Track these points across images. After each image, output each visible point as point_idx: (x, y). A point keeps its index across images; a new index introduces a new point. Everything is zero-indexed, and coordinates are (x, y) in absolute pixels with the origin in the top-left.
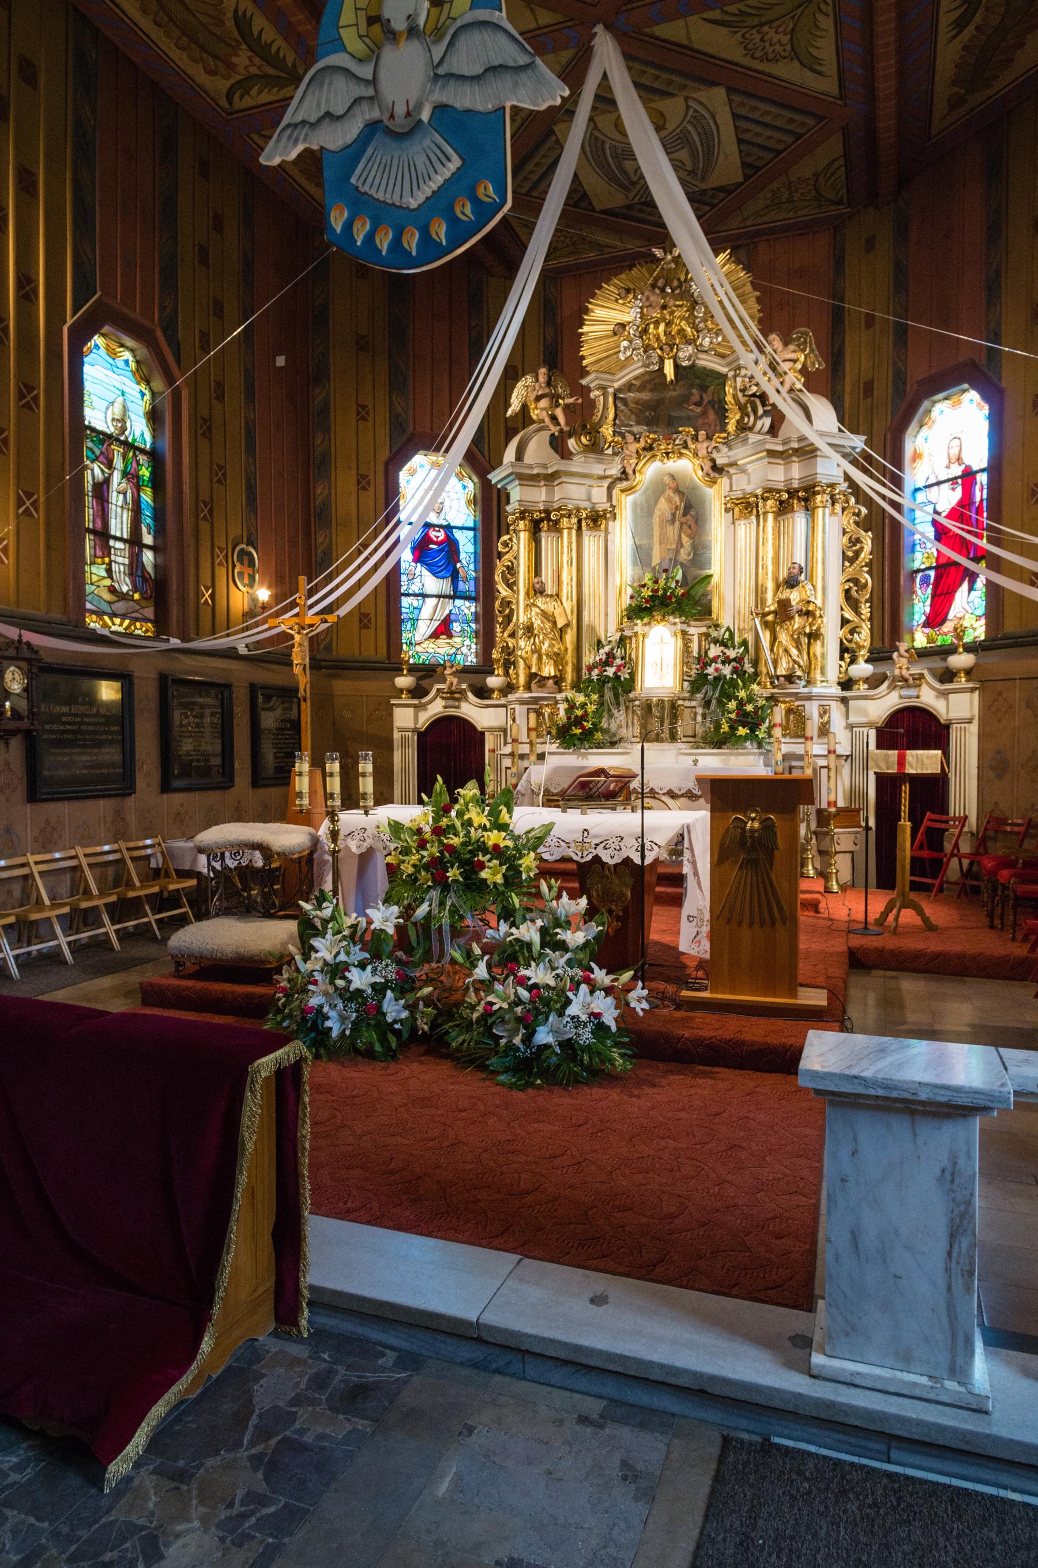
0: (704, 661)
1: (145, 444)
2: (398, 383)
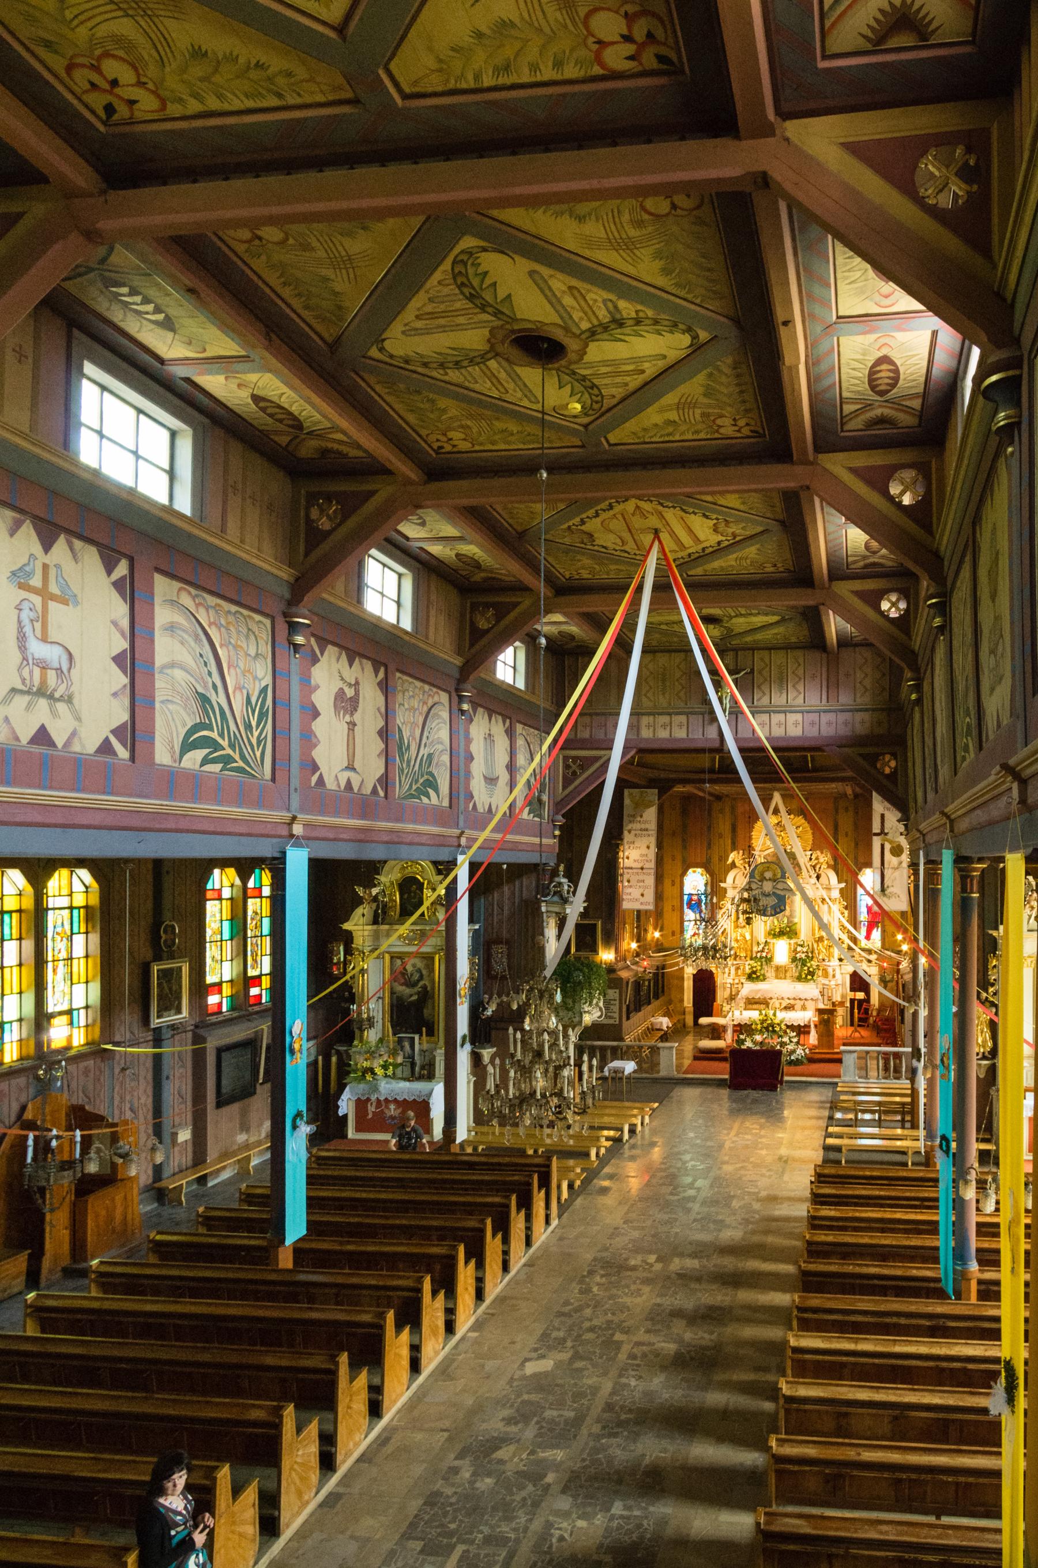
0: (795, 951)
1: (631, 794)
2: (685, 847)
